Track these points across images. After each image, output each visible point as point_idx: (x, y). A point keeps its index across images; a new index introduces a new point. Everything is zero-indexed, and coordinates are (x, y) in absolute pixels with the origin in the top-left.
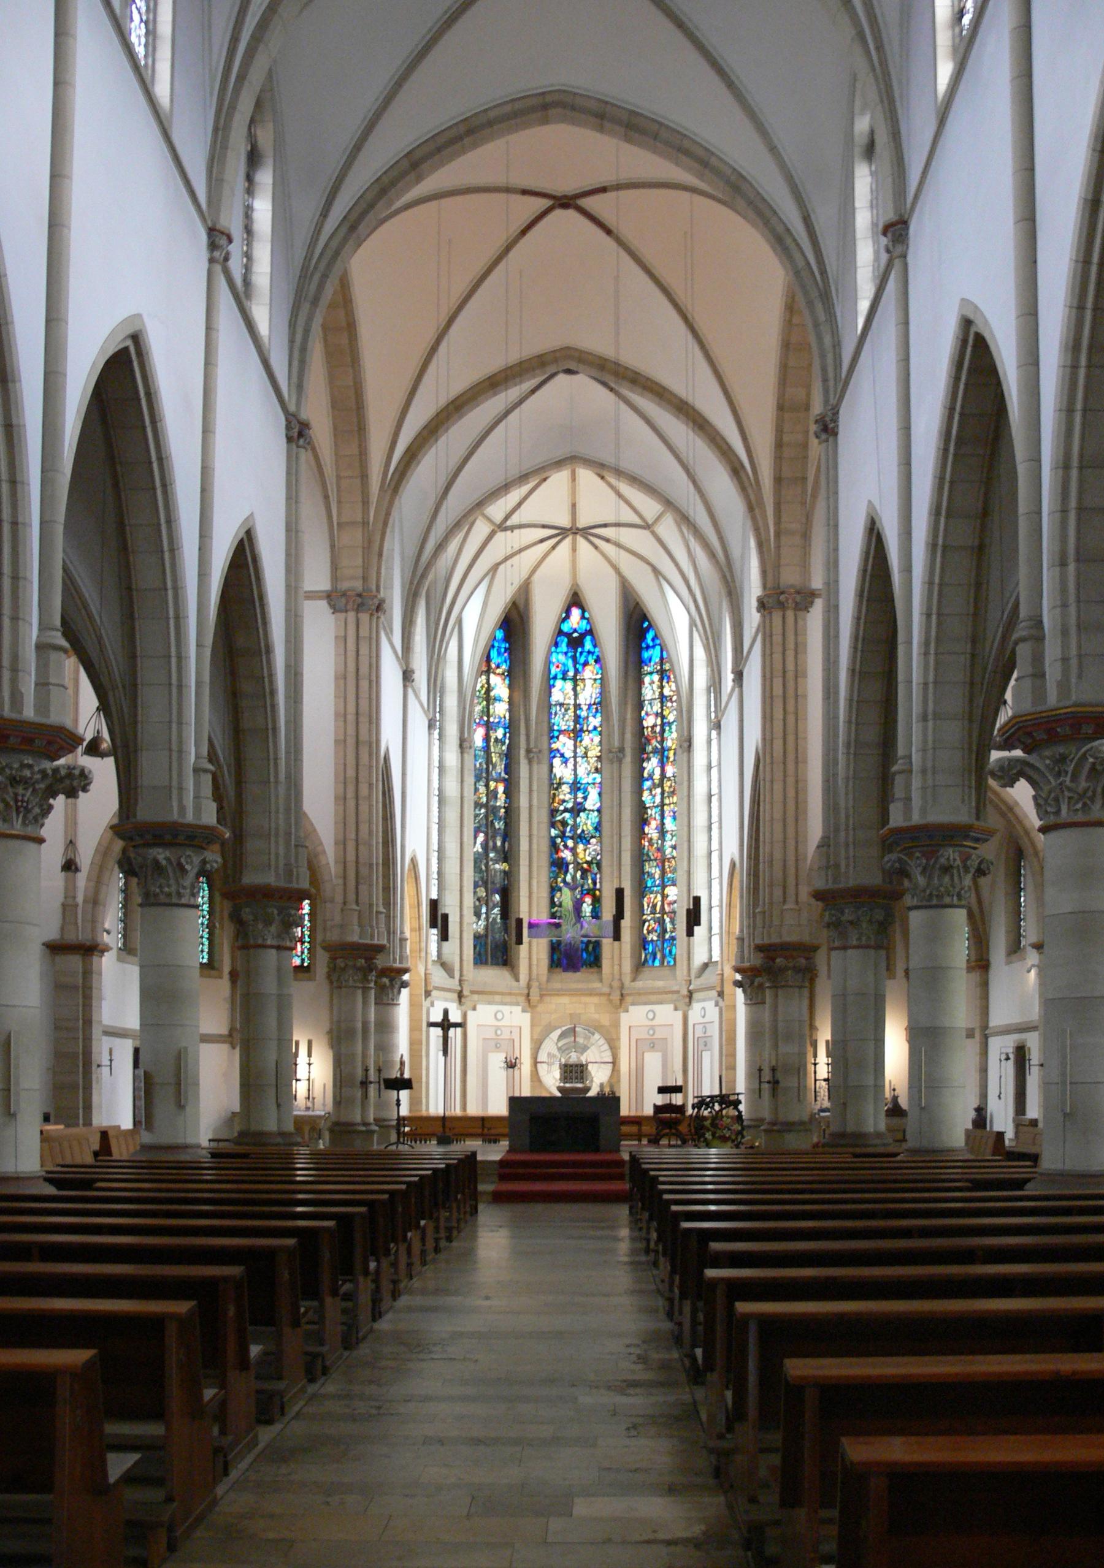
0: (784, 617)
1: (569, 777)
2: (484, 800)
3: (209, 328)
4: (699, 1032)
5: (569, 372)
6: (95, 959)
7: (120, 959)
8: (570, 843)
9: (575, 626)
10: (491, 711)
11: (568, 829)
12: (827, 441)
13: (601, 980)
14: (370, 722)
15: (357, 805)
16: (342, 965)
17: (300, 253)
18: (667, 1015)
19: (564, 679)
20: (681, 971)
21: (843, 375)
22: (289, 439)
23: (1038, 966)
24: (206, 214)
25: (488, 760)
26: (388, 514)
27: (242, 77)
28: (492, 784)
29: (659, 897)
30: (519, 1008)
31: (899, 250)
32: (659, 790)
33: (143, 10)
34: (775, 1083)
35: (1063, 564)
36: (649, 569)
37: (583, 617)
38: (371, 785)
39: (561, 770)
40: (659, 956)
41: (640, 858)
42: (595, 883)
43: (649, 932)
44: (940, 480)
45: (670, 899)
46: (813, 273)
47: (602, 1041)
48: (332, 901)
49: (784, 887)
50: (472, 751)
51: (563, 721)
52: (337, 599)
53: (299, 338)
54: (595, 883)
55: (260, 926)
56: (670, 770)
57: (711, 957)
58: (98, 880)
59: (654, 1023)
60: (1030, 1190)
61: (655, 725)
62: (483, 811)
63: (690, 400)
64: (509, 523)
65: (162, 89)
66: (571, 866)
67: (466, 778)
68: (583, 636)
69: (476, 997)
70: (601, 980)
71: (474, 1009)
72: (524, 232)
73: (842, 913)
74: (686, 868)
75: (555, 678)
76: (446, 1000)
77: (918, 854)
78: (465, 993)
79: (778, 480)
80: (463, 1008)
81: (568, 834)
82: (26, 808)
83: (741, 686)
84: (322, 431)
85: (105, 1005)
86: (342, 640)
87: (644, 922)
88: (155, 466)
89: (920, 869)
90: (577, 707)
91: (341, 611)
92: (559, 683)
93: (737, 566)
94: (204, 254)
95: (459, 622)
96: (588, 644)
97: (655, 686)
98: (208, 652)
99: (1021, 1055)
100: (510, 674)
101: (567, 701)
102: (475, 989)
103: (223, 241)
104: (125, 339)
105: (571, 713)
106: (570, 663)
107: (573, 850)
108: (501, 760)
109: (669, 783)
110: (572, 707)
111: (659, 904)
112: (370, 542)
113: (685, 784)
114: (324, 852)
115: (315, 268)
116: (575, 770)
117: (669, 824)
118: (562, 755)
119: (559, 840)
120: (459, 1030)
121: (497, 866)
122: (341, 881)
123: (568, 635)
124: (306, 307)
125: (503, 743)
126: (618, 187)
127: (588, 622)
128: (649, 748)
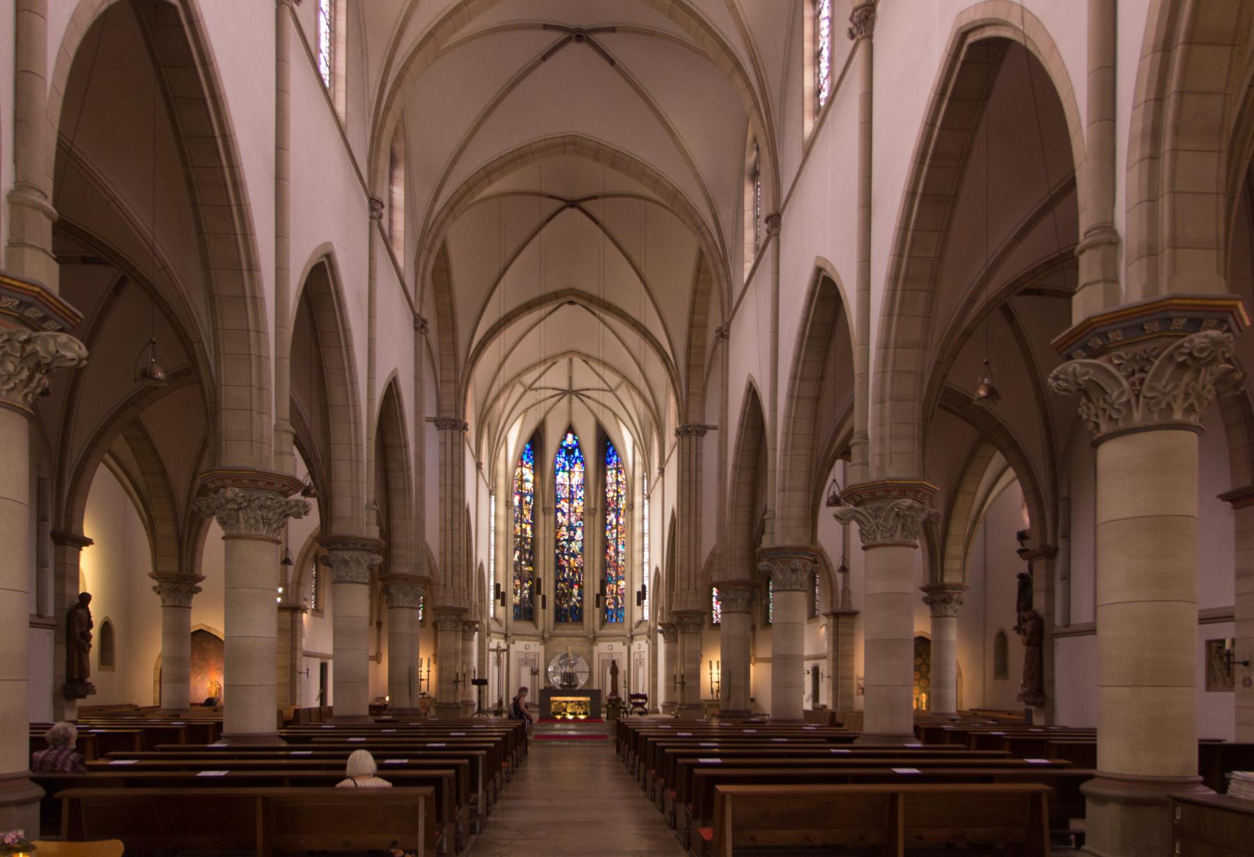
0: (690, 439)
1: (566, 523)
2: (519, 534)
3: (371, 257)
4: (637, 656)
5: (571, 303)
6: (298, 614)
7: (313, 615)
8: (566, 557)
9: (570, 443)
10: (523, 487)
11: (565, 550)
12: (723, 342)
13: (583, 629)
14: (460, 489)
15: (452, 534)
16: (443, 619)
17: (420, 222)
18: (618, 648)
19: (564, 471)
20: (627, 625)
21: (733, 308)
22: (416, 329)
23: (826, 625)
24: (368, 188)
25: (522, 513)
26: (469, 376)
27: (387, 109)
28: (524, 526)
29: (615, 586)
30: (538, 643)
31: (775, 230)
32: (615, 531)
33: (328, 59)
34: (683, 683)
35: (882, 401)
36: (611, 413)
37: (574, 439)
38: (460, 523)
39: (560, 518)
40: (615, 616)
41: (605, 566)
42: (580, 578)
43: (609, 604)
44: (797, 359)
45: (621, 587)
46: (717, 248)
47: (583, 661)
48: (438, 584)
49: (689, 580)
50: (513, 508)
51: (564, 493)
52: (440, 423)
53: (420, 272)
54: (580, 578)
55: (401, 596)
56: (621, 521)
57: (643, 617)
58: (300, 572)
59: (612, 652)
60: (857, 743)
61: (613, 496)
62: (519, 539)
63: (642, 322)
64: (534, 386)
65: (341, 107)
66: (567, 569)
67: (509, 522)
68: (575, 447)
69: (514, 637)
70: (583, 629)
71: (514, 643)
72: (548, 221)
73: (728, 594)
74: (630, 570)
75: (558, 470)
76: (498, 638)
77: (778, 563)
78: (509, 634)
79: (688, 365)
80: (508, 642)
81: (565, 552)
82: (269, 523)
83: (663, 476)
84: (432, 326)
85: (304, 640)
86: (443, 444)
87: (607, 599)
88: (341, 334)
89: (780, 570)
90: (571, 486)
91: (443, 429)
92: (561, 473)
93: (662, 412)
94: (367, 214)
95: (506, 439)
96: (577, 454)
97: (613, 476)
98: (373, 443)
99: (816, 672)
100: (534, 468)
101: (565, 483)
102: (515, 632)
103: (378, 206)
104: (322, 256)
105: (567, 489)
106: (567, 463)
107: (568, 561)
108: (529, 513)
109: (621, 527)
110: (568, 486)
111: (615, 589)
112: (459, 391)
113: (630, 527)
114: (433, 558)
115: (430, 231)
116: (569, 519)
117: (621, 548)
118: (562, 511)
119: (560, 556)
120: (505, 653)
121: (526, 569)
122: (443, 574)
123: (566, 448)
124: (424, 253)
125: (530, 504)
126: (605, 196)
127: (577, 442)
128: (610, 509)
